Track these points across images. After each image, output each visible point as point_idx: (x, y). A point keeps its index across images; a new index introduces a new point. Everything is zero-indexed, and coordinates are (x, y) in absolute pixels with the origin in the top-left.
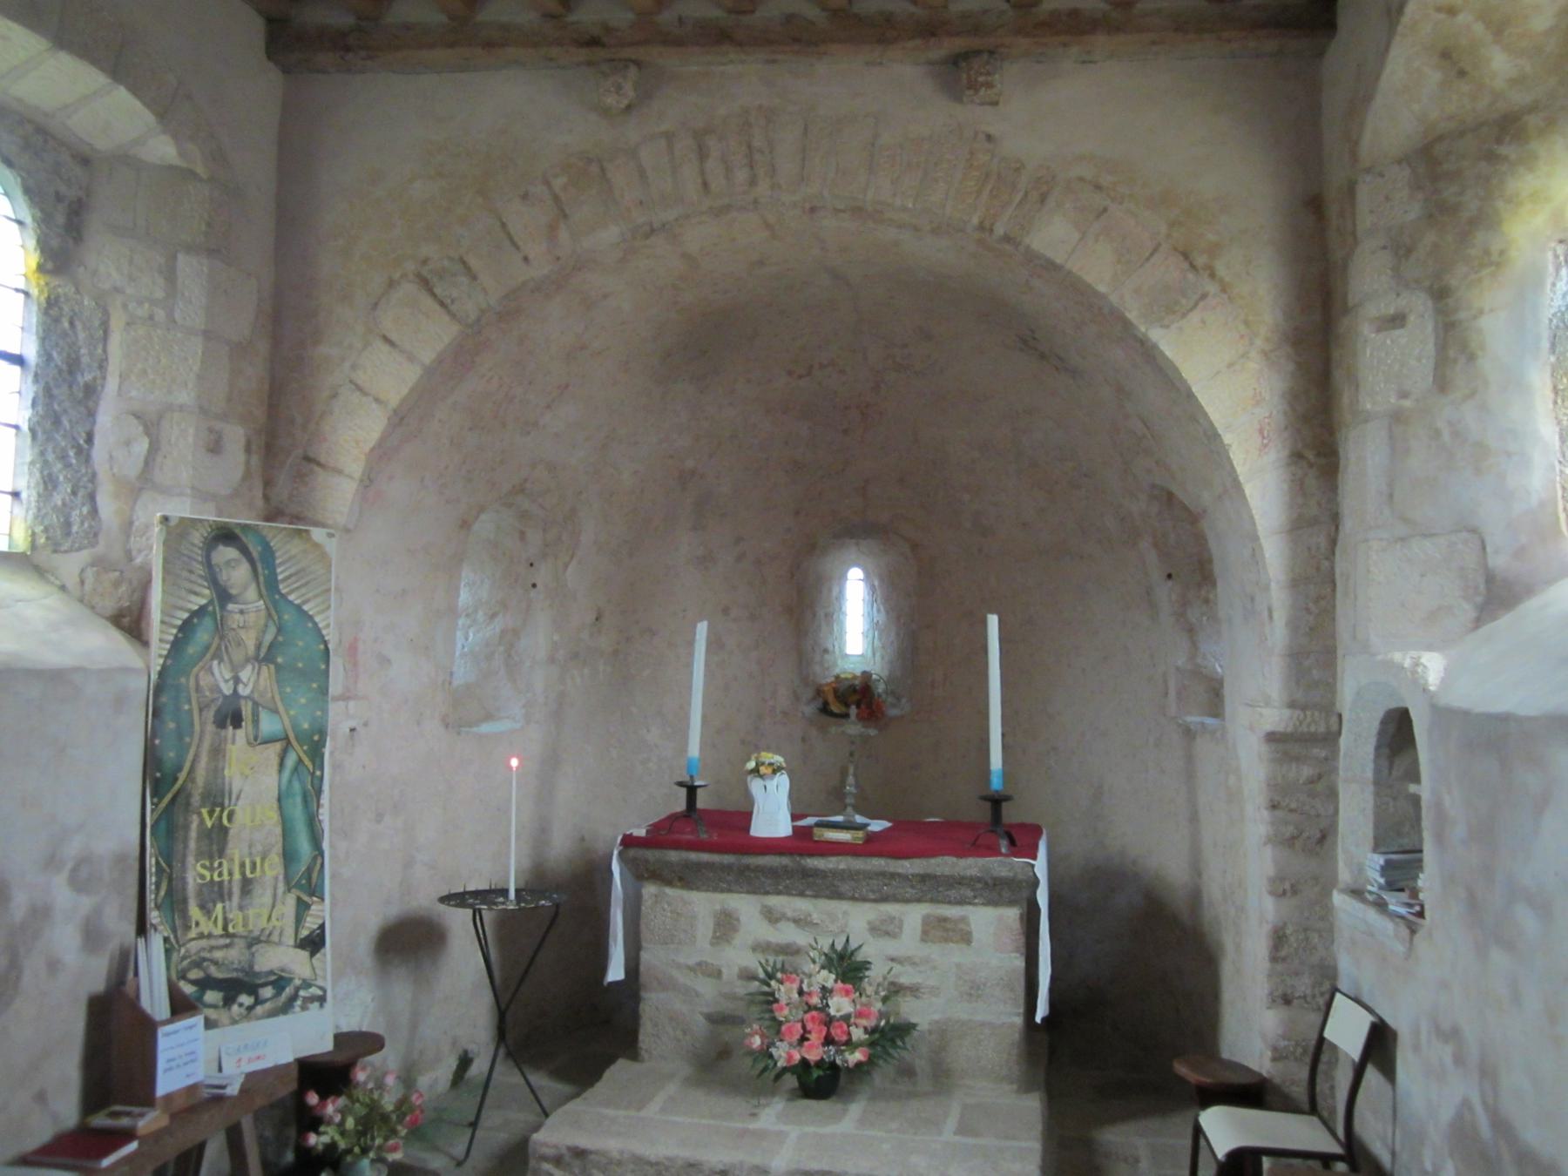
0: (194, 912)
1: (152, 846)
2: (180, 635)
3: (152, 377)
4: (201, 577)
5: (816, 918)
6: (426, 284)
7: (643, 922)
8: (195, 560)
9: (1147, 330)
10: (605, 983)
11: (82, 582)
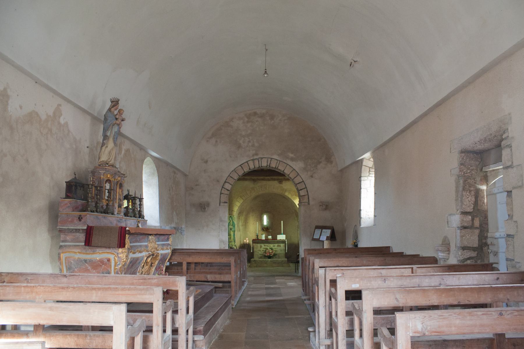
6: (241, 197)
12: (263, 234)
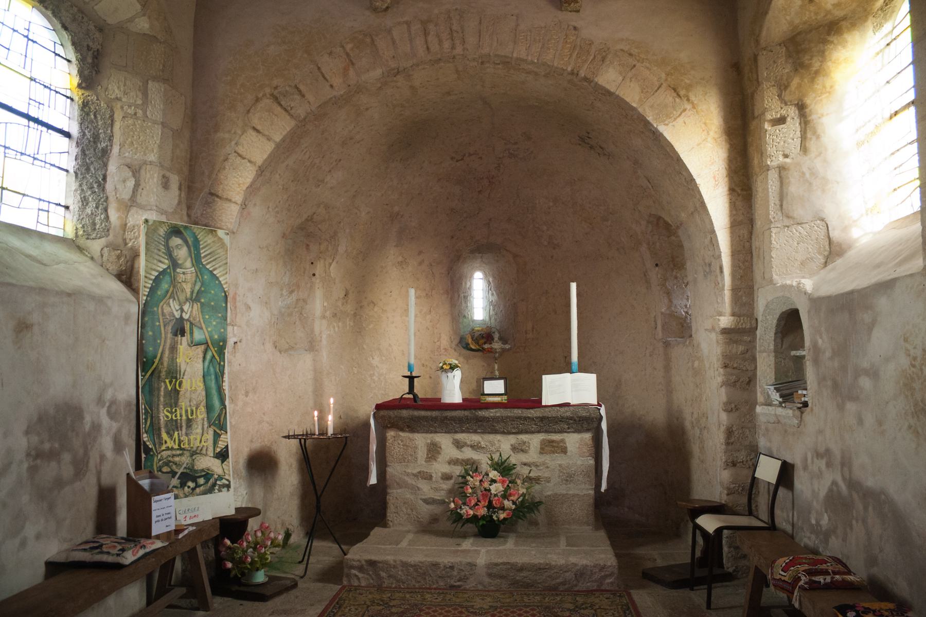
0: (165, 436)
1: (142, 399)
2: (154, 284)
3: (136, 146)
4: (163, 253)
5: (483, 444)
6: (276, 99)
7: (388, 451)
8: (161, 244)
9: (657, 126)
10: (368, 485)
11: (102, 256)
12: (452, 368)
